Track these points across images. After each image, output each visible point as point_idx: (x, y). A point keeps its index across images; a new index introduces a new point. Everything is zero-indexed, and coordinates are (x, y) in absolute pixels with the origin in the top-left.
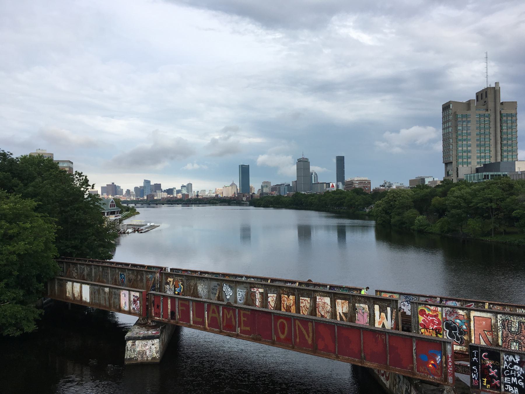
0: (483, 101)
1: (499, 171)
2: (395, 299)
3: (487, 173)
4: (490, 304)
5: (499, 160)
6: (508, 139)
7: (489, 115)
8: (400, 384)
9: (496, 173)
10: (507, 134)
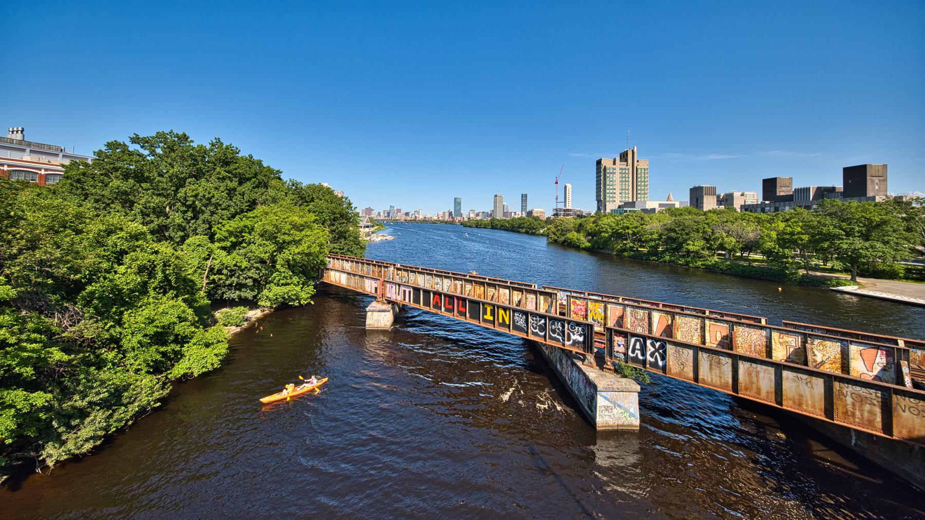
1: (635, 207)
2: (738, 354)
6: (641, 182)
7: (629, 169)
10: (640, 185)
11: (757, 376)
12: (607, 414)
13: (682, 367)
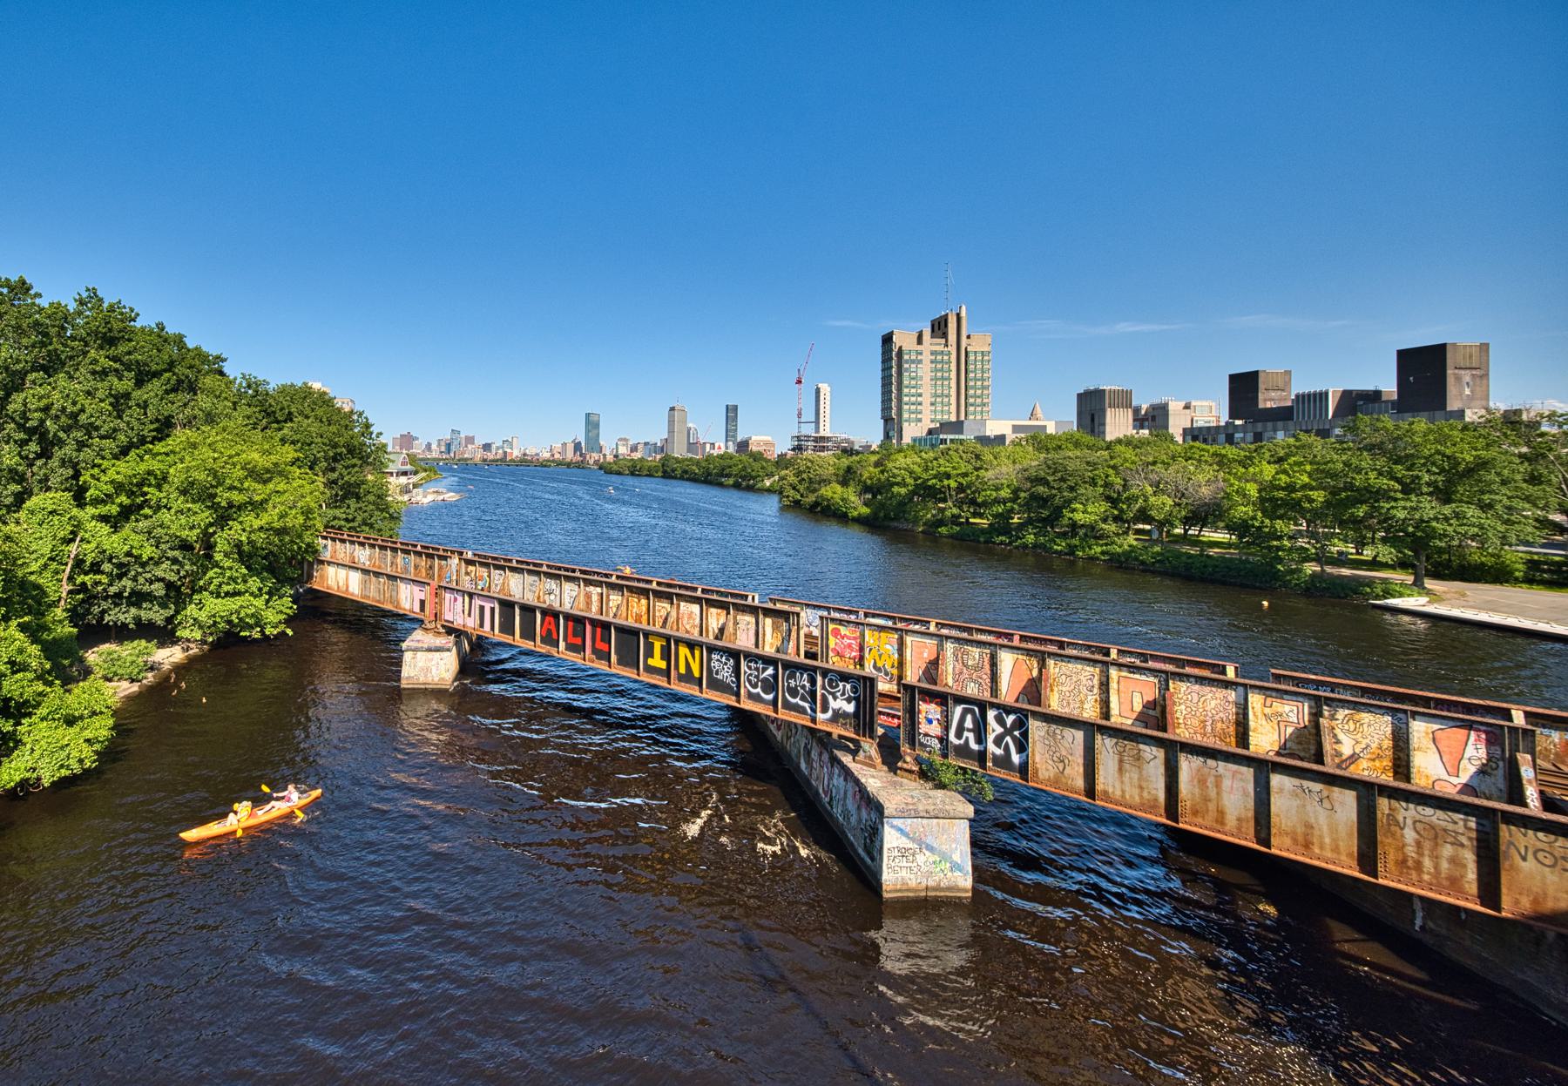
0: (940, 333)
1: (962, 433)
3: (945, 437)
4: (937, 624)
5: (962, 418)
7: (949, 354)
8: (797, 737)
9: (957, 437)
11: (1218, 785)
12: (905, 864)
13: (1061, 766)
